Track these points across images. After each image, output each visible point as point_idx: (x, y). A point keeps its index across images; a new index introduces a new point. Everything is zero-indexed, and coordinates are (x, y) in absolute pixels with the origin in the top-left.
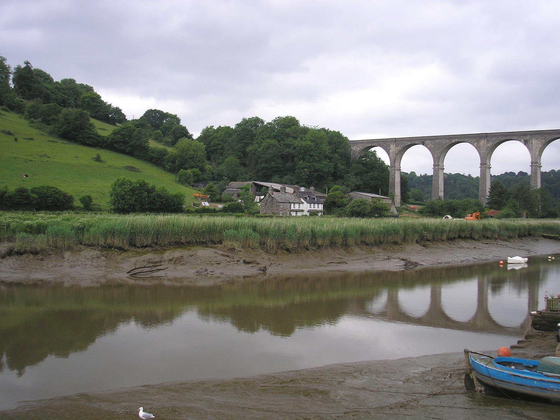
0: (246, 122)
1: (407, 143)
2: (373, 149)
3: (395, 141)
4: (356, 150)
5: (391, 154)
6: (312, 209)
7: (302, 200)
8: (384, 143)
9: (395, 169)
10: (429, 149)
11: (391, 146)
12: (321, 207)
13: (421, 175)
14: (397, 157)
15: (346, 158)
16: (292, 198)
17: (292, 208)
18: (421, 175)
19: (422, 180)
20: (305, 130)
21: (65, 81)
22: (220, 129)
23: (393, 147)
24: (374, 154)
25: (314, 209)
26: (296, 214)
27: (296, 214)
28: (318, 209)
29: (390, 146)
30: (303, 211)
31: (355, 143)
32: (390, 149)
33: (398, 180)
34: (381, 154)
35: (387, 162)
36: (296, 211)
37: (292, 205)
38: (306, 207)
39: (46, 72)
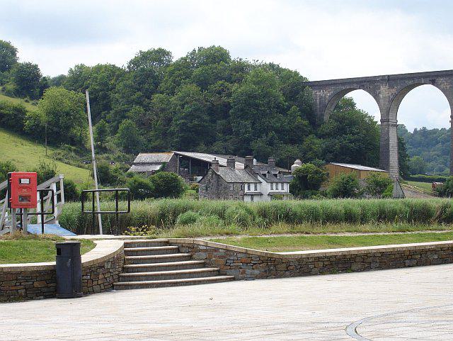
0: (145, 57)
1: (404, 83)
2: (348, 96)
3: (390, 80)
4: (325, 97)
5: (381, 101)
6: (275, 191)
7: (260, 178)
8: (368, 84)
9: (389, 125)
10: (443, 91)
11: (382, 88)
12: (286, 188)
13: (415, 130)
14: (390, 108)
15: (310, 114)
16: (246, 178)
17: (246, 190)
18: (415, 130)
19: (418, 138)
20: (241, 68)
21: (28, 66)
22: (99, 68)
23: (384, 91)
24: (351, 104)
25: (277, 191)
26: (252, 199)
27: (252, 199)
28: (283, 191)
29: (379, 88)
30: (261, 194)
31: (323, 85)
32: (379, 93)
33: (393, 142)
34: (364, 102)
35: (377, 116)
36: (252, 196)
37: (246, 186)
38: (266, 187)
39: (145, 50)
